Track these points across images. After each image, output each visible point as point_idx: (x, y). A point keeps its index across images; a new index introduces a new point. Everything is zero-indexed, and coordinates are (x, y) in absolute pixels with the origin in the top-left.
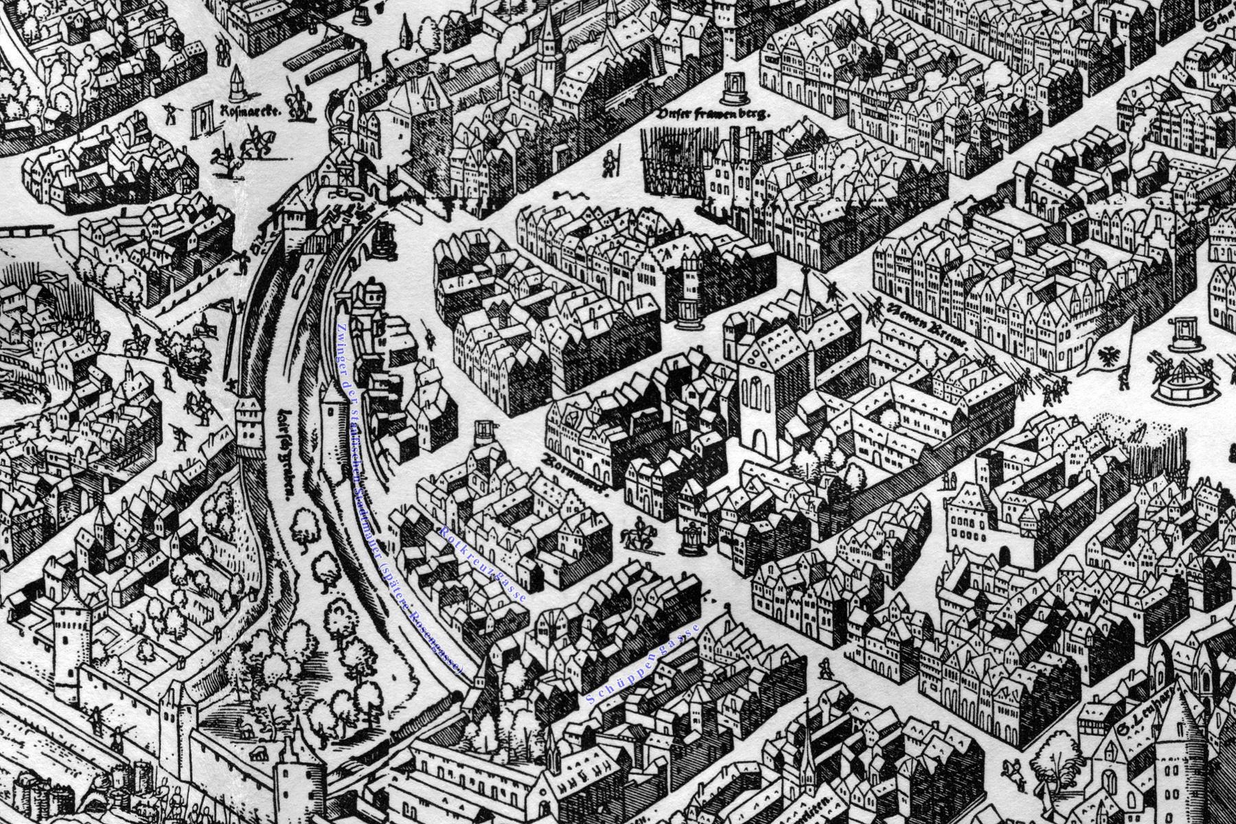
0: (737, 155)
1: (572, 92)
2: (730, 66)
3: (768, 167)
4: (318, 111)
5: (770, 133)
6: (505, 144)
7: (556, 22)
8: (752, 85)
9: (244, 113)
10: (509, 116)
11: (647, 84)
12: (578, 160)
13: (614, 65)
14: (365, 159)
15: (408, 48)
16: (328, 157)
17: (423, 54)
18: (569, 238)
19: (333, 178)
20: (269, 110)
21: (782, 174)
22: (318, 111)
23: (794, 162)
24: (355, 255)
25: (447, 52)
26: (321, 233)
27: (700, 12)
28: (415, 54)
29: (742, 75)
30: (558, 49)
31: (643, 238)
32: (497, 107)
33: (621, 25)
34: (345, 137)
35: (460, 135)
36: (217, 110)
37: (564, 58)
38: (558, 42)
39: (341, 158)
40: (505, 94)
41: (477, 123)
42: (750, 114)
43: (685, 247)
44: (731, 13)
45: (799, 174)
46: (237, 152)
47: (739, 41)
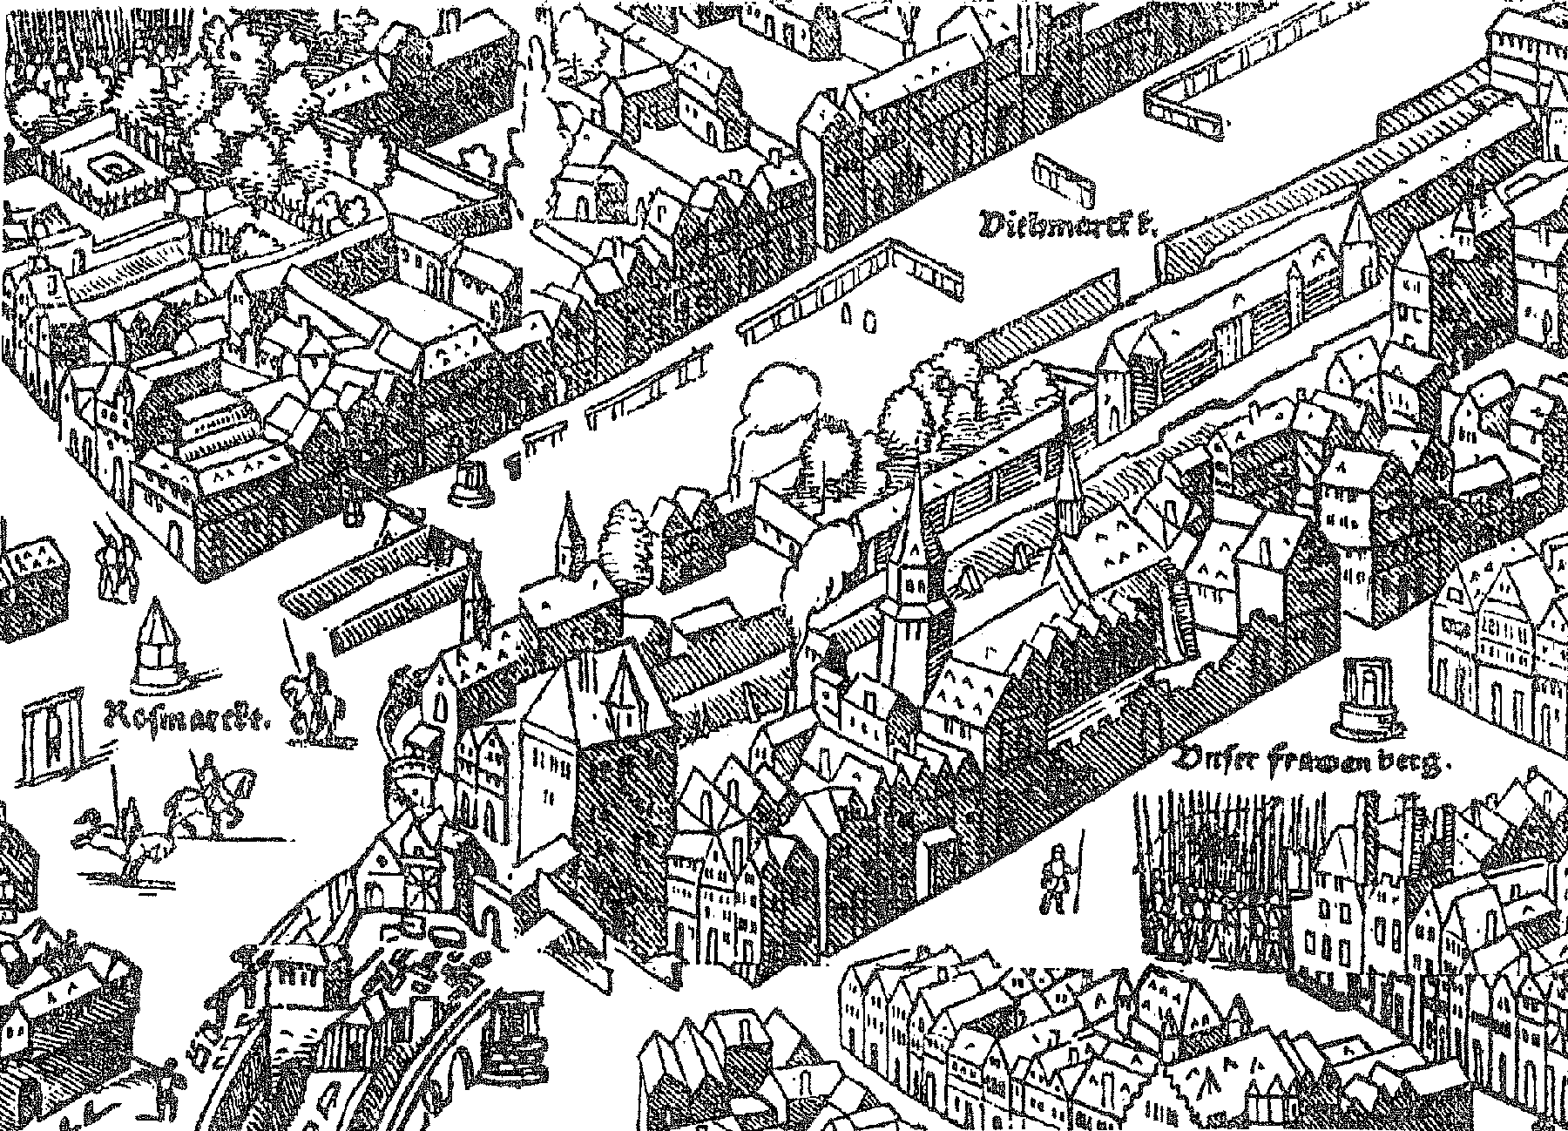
0: (1371, 866)
1: (969, 699)
2: (1356, 641)
3: (1445, 895)
4: (360, 721)
5: (1448, 809)
6: (799, 824)
7: (935, 517)
8: (1409, 689)
9: (175, 722)
10: (811, 756)
11: (1150, 678)
12: (981, 866)
13: (1072, 632)
14: (472, 840)
15: (574, 577)
16: (381, 837)
17: (607, 593)
18: (967, 1036)
19: (393, 892)
20: (243, 716)
21: (1475, 910)
22: (360, 721)
23: (1504, 884)
24: (440, 1074)
25: (665, 589)
26: (359, 1017)
27: (1284, 507)
28: (590, 593)
29: (1385, 664)
30: (935, 588)
31: (1151, 1041)
32: (780, 732)
33: (1089, 532)
34: (423, 786)
35: (692, 799)
36: (94, 711)
37: (951, 611)
38: (936, 569)
39: (414, 840)
40: (804, 699)
41: (735, 772)
42: (1404, 762)
43: (1256, 1065)
44: (1360, 510)
45: (1515, 914)
46: (154, 820)
47: (1377, 582)
